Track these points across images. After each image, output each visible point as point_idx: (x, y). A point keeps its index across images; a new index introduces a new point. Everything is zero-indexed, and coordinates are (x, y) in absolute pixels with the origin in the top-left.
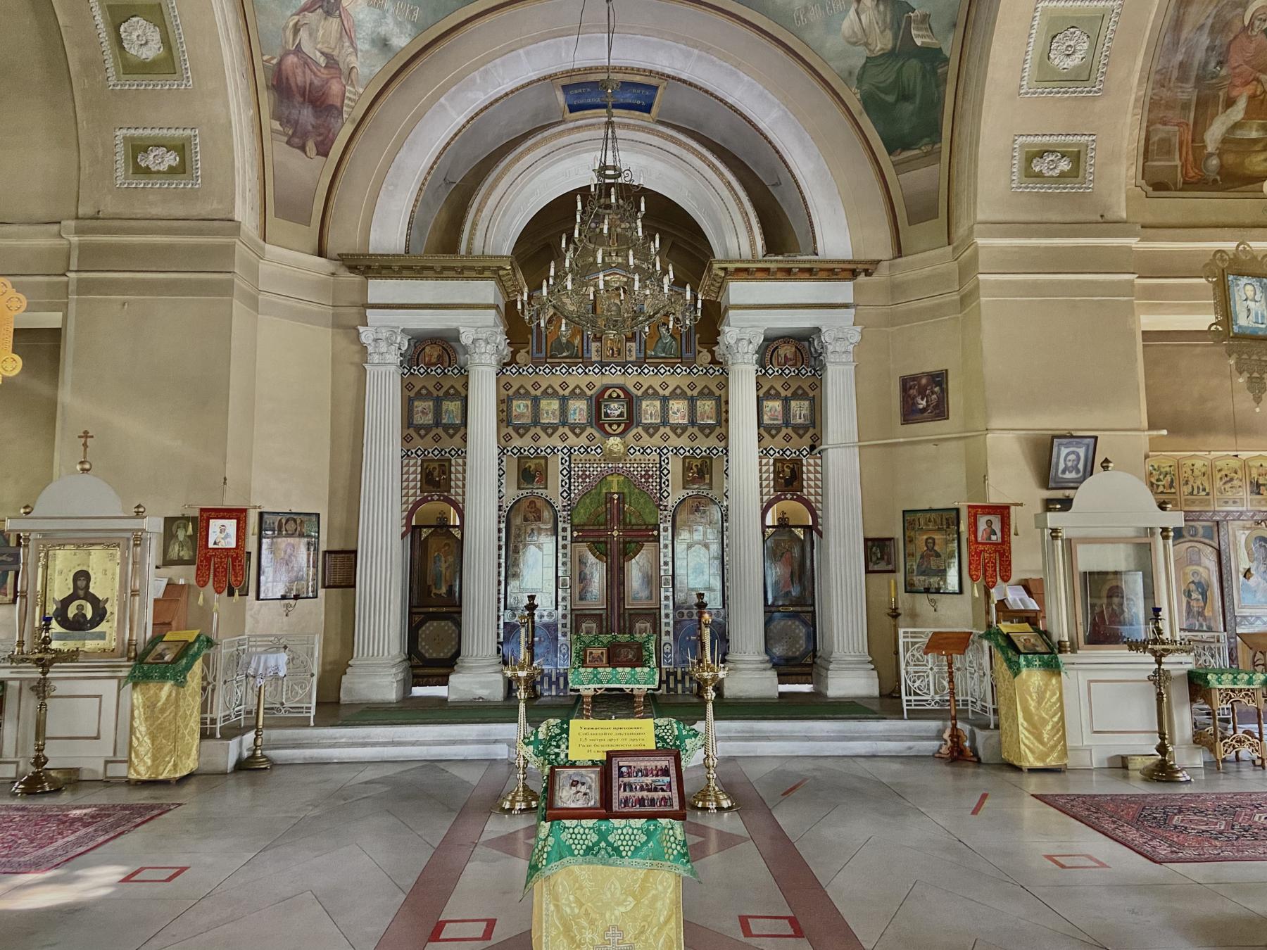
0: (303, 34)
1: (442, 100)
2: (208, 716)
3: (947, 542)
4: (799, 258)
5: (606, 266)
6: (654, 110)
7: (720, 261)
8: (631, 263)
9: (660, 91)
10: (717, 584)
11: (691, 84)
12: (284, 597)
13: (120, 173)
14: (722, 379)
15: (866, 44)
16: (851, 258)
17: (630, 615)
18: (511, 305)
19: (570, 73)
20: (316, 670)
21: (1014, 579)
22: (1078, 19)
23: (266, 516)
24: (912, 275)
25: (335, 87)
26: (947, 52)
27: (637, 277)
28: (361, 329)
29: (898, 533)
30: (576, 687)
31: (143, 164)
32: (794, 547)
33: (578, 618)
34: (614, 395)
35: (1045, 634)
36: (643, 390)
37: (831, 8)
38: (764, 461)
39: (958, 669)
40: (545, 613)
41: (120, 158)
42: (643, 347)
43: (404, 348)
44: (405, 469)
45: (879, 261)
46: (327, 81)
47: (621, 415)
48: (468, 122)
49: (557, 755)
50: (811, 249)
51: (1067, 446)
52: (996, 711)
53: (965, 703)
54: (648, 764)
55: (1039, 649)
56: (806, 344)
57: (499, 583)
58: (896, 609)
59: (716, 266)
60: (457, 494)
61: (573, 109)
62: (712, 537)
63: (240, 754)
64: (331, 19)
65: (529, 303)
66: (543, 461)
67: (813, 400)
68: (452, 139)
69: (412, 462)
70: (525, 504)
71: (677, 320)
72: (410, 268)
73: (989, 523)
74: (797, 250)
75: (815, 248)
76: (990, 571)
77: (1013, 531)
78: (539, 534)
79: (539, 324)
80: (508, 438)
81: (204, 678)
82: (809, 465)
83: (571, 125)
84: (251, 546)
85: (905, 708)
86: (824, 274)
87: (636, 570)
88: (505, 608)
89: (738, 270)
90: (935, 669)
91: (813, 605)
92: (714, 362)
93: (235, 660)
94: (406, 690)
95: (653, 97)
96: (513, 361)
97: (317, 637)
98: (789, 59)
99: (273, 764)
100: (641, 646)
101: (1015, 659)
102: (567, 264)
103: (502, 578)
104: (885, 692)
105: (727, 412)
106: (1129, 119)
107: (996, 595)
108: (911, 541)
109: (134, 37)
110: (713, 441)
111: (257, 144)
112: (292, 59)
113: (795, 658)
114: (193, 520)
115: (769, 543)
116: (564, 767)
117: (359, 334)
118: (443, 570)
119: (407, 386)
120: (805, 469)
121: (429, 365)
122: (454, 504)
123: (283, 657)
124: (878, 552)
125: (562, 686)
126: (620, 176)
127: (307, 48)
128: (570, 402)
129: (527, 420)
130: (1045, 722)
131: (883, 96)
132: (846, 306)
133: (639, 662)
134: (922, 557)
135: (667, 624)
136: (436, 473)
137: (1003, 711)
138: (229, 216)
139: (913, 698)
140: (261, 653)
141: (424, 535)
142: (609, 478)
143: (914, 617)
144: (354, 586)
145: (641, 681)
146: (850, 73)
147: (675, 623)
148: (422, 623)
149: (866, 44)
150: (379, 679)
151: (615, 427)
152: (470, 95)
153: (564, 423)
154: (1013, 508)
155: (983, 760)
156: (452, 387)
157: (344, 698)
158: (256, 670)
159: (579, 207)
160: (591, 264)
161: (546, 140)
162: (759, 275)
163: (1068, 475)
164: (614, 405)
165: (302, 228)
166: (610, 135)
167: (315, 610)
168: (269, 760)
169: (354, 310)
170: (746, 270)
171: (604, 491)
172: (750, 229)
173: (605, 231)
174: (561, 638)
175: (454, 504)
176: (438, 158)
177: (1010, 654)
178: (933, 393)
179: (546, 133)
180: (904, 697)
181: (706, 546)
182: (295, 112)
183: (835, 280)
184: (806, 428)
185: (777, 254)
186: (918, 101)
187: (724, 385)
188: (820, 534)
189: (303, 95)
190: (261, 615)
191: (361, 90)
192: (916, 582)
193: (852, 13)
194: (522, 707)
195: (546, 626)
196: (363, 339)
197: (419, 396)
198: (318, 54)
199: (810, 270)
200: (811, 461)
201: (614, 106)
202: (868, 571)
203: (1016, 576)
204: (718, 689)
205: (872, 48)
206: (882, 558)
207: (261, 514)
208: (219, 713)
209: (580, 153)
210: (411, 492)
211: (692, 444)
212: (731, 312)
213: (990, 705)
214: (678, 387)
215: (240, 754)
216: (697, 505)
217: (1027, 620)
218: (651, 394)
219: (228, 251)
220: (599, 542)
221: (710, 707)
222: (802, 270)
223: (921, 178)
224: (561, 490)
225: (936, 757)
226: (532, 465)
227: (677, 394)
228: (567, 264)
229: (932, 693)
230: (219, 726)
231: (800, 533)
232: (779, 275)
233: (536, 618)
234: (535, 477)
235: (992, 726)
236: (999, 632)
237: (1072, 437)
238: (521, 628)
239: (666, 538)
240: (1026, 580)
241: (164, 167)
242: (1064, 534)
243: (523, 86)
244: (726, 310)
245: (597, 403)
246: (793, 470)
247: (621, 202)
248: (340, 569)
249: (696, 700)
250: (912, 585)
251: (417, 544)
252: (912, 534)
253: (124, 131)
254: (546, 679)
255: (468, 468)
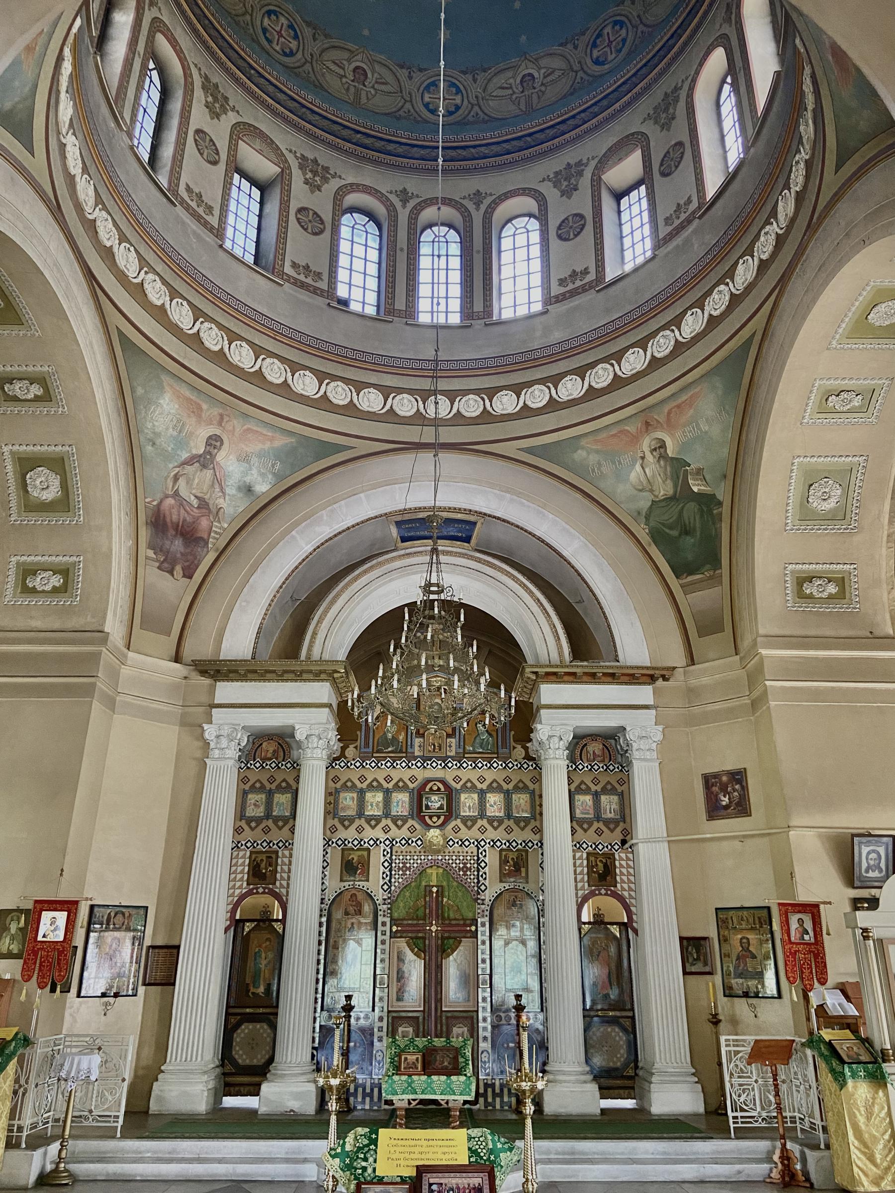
0: (182, 482)
1: (293, 533)
2: (16, 1122)
3: (761, 942)
4: (602, 664)
5: (430, 668)
6: (474, 540)
7: (532, 666)
8: (451, 665)
9: (478, 525)
10: (535, 985)
11: (504, 521)
12: (104, 995)
13: (10, 592)
14: (535, 773)
15: (651, 491)
16: (649, 665)
17: (447, 1018)
18: (342, 704)
19: (404, 511)
20: (128, 1075)
21: (831, 982)
22: (829, 471)
23: (96, 909)
24: (705, 680)
25: (204, 523)
26: (720, 497)
27: (456, 677)
28: (206, 726)
29: (712, 932)
30: (389, 1097)
31: (31, 585)
32: (611, 944)
33: (395, 1020)
34: (435, 788)
35: (867, 1042)
36: (461, 783)
37: (620, 463)
38: (578, 855)
39: (784, 1082)
40: (362, 1015)
41: (12, 579)
42: (462, 743)
43: (243, 744)
44: (234, 861)
45: (674, 668)
46: (198, 518)
47: (441, 808)
48: (315, 550)
49: (364, 1169)
50: (612, 657)
51: (868, 844)
52: (825, 1129)
53: (793, 1120)
54: (459, 1181)
55: (862, 1058)
56: (613, 742)
57: (317, 981)
58: (716, 1014)
59: (528, 670)
60: (282, 886)
61: (404, 539)
62: (529, 933)
63: (43, 1167)
64: (205, 471)
65: (359, 701)
66: (365, 853)
67: (621, 795)
68: (300, 564)
69: (241, 854)
70: (347, 896)
71: (492, 717)
72: (255, 672)
73: (801, 922)
74: (598, 657)
75: (617, 656)
76: (806, 972)
77: (824, 932)
78: (359, 928)
79: (367, 720)
80: (333, 830)
81: (17, 1081)
82: (621, 859)
83: (402, 552)
84: (79, 941)
85: (732, 1126)
86: (626, 679)
87: (453, 967)
88: (322, 1009)
89: (548, 674)
90: (760, 1081)
91: (632, 1009)
92: (528, 757)
93: (50, 1060)
94: (217, 1100)
95: (472, 530)
96: (343, 755)
97: (132, 1038)
98: (587, 502)
99: (75, 1179)
100: (457, 1052)
101: (839, 1068)
102: (394, 666)
103: (321, 976)
104: (709, 1110)
105: (541, 805)
106: (884, 551)
107: (814, 1002)
108: (726, 940)
109: (38, 482)
110: (528, 835)
111: (132, 568)
112: (170, 501)
113: (616, 1069)
114: (27, 912)
115: (586, 940)
116: (371, 1183)
117: (203, 731)
118: (262, 967)
119: (243, 780)
120: (617, 863)
121: (264, 760)
122: (277, 896)
123: (96, 1059)
124: (693, 948)
125: (376, 1099)
126: (442, 591)
127: (184, 492)
128: (394, 794)
129: (352, 812)
130: (875, 1140)
131: (667, 531)
132: (646, 707)
133: (455, 1070)
134: (738, 958)
135: (485, 1029)
136: (263, 865)
137: (832, 1129)
138: (100, 628)
139: (739, 1114)
140: (75, 1054)
141: (247, 930)
142: (429, 871)
143: (734, 1022)
144: (174, 984)
145: (454, 1091)
146: (639, 513)
147: (494, 1027)
148: (238, 1026)
149: (651, 491)
150: (187, 1086)
151: (435, 819)
152: (317, 529)
153: (387, 815)
154: (822, 907)
155: (816, 1186)
156: (284, 780)
157: (154, 1107)
158: (69, 1073)
159: (407, 617)
160: (415, 666)
161: (380, 564)
162: (566, 678)
163: (871, 874)
164: (434, 798)
165: (163, 638)
166: (434, 561)
167: (134, 1009)
168: (71, 1175)
169: (201, 709)
170: (555, 674)
171: (424, 884)
172: (558, 639)
173: (429, 637)
174: (376, 1044)
175: (277, 896)
176: (286, 579)
177: (835, 1063)
178: (734, 790)
179: (380, 559)
180: (730, 1114)
181: (523, 943)
182: (168, 543)
183: (635, 684)
184: (616, 823)
185: (582, 660)
186: (698, 534)
187: (537, 779)
188: (636, 931)
189: (176, 530)
190: (81, 1014)
191: (226, 525)
192: (735, 986)
193: (638, 467)
194: (333, 1118)
195: (362, 1030)
196: (206, 736)
197: (253, 789)
198: (193, 498)
199: (613, 675)
200: (623, 855)
201: (439, 538)
202: (685, 973)
203: (832, 980)
204: (538, 1104)
205: (656, 493)
206: (698, 959)
207: (92, 907)
208: (27, 1120)
209: (409, 574)
210: (238, 884)
211: (508, 837)
212: (543, 712)
213: (818, 1122)
214: (495, 781)
215: (43, 1167)
216: (513, 900)
217: (848, 1026)
218: (468, 787)
219: (95, 657)
220: (417, 938)
221: (529, 1122)
222: (604, 674)
223: (703, 598)
224: (381, 883)
225: (767, 1182)
226: (355, 856)
227: (495, 787)
228: (394, 666)
229: (759, 1109)
230: (25, 1134)
231: (615, 930)
232: (585, 678)
233: (352, 1020)
234: (357, 869)
235: (822, 1146)
236: (821, 1039)
237: (870, 835)
238: (337, 1032)
239: (483, 932)
240: (843, 984)
241: (48, 588)
242: (875, 933)
243: (363, 522)
244: (538, 710)
245: (419, 796)
246: (605, 865)
247: (443, 613)
248: (161, 967)
249: (514, 1117)
250: (731, 988)
251: (239, 939)
252: (726, 933)
253: (19, 558)
254: (360, 1090)
255: (294, 860)
